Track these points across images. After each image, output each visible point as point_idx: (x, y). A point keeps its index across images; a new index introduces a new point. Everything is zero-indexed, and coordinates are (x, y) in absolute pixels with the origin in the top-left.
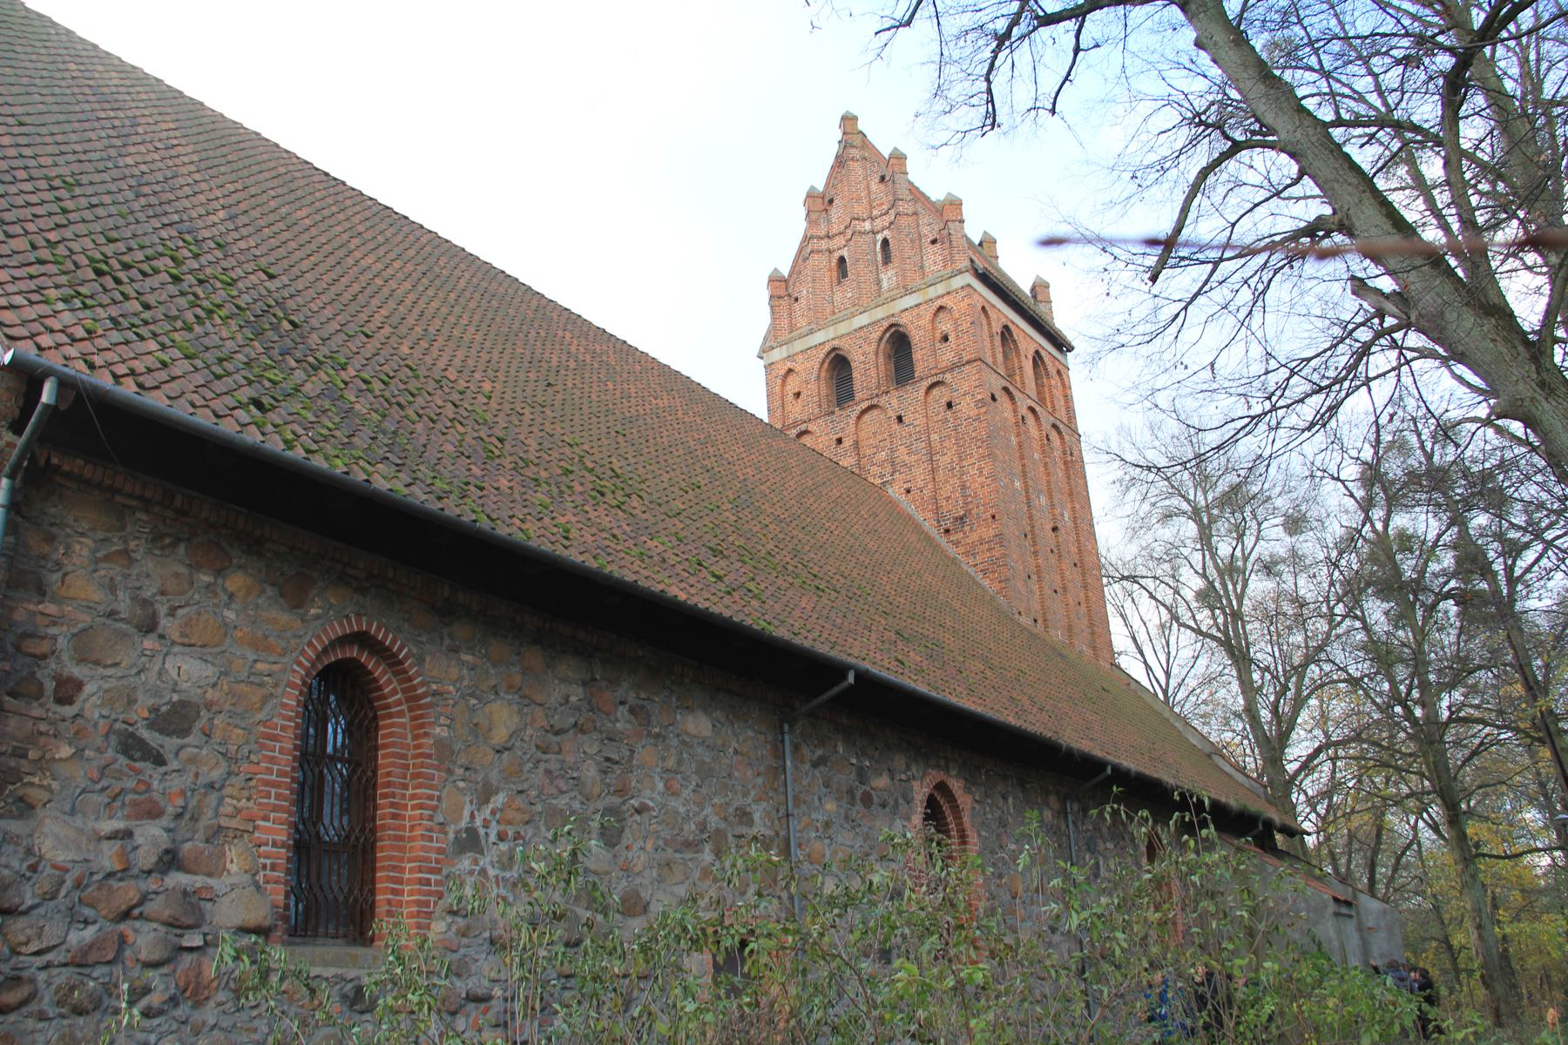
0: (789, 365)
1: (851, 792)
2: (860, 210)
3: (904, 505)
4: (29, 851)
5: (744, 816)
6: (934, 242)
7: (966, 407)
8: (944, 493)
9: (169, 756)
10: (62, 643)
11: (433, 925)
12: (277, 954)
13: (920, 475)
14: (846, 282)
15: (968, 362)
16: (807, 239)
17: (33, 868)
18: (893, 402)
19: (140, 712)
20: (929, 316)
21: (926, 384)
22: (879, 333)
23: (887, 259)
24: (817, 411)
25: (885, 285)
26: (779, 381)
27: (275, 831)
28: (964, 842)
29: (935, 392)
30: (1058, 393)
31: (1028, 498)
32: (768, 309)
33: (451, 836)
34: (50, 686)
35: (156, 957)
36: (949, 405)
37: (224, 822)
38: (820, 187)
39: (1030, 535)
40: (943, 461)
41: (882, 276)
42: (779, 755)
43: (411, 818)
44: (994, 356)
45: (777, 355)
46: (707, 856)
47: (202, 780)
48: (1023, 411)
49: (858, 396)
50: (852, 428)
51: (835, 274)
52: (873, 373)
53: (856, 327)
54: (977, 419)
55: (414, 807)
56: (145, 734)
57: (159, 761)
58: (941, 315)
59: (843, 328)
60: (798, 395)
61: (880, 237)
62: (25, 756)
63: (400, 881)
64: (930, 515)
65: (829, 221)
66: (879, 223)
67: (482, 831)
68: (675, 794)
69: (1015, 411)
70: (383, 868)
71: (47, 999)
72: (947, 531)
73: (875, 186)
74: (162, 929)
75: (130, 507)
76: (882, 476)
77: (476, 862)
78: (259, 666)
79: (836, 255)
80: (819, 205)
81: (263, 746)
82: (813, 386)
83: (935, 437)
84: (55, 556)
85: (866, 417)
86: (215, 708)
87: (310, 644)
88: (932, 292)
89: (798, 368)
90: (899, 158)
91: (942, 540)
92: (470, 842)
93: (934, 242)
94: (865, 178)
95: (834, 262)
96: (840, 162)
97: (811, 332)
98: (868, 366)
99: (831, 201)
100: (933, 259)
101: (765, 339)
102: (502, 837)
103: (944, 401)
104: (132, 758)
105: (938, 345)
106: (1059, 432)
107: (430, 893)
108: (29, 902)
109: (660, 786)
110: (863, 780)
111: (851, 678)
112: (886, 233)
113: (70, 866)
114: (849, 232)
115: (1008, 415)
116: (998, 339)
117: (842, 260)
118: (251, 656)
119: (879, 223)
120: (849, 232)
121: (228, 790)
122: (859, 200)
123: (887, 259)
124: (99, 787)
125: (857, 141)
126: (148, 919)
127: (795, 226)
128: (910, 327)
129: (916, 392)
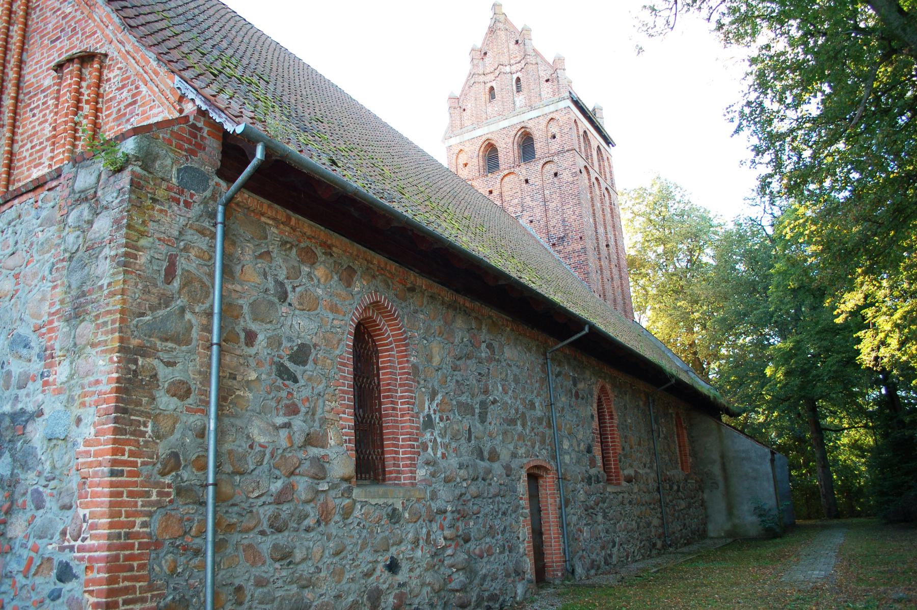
0: (461, 147)
1: (571, 391)
2: (505, 60)
3: (529, 229)
4: (248, 437)
5: (532, 406)
6: (547, 81)
7: (566, 176)
8: (552, 223)
9: (299, 377)
10: (246, 309)
11: (418, 471)
12: (357, 493)
13: (538, 213)
14: (494, 101)
15: (568, 151)
16: (472, 75)
17: (251, 447)
18: (523, 171)
19: (285, 353)
20: (544, 123)
21: (542, 162)
22: (515, 132)
23: (519, 89)
24: (477, 174)
25: (518, 104)
26: (455, 157)
27: (347, 419)
28: (612, 419)
29: (548, 167)
30: (607, 170)
31: (596, 228)
32: (448, 114)
33: (421, 419)
34: (242, 335)
35: (309, 497)
36: (556, 174)
37: (327, 415)
38: (479, 45)
39: (598, 249)
40: (552, 206)
41: (516, 99)
42: (544, 370)
43: (401, 410)
44: (580, 148)
45: (454, 141)
46: (519, 427)
47: (316, 391)
48: (593, 180)
49: (502, 167)
50: (498, 185)
51: (488, 96)
52: (511, 154)
53: (501, 128)
54: (573, 183)
55: (402, 404)
56: (288, 364)
57: (296, 381)
58: (551, 123)
59: (493, 128)
60: (466, 165)
61: (515, 76)
62: (235, 378)
63: (397, 446)
64: (544, 235)
65: (484, 65)
66: (514, 68)
67: (433, 416)
68: (506, 393)
69: (589, 179)
70: (389, 439)
71: (265, 525)
72: (554, 245)
73: (512, 45)
74: (310, 481)
75: (268, 224)
76: (516, 213)
77: (432, 434)
78: (335, 322)
79: (489, 85)
80: (478, 55)
81: (340, 370)
82: (475, 160)
83: (546, 192)
84: (236, 255)
85: (506, 179)
86: (318, 348)
87: (357, 309)
88: (546, 110)
89: (466, 149)
90: (526, 31)
91: (551, 250)
92: (429, 423)
93: (547, 81)
94: (507, 41)
95: (487, 89)
96: (492, 31)
97: (474, 129)
98: (507, 151)
99: (485, 54)
100: (546, 90)
101: (446, 133)
102: (441, 419)
103: (553, 172)
104: (282, 379)
105: (550, 140)
106: (608, 192)
107: (414, 453)
108: (252, 467)
109: (500, 388)
110: (575, 384)
111: (587, 329)
112: (519, 74)
113: (267, 445)
114: (497, 72)
115: (587, 181)
116: (582, 138)
117: (492, 88)
118: (331, 316)
119: (514, 68)
120: (497, 72)
121: (326, 396)
122: (503, 53)
123: (519, 89)
124: (270, 397)
125: (502, 18)
126: (303, 475)
127: (465, 67)
128: (534, 129)
129: (535, 166)
